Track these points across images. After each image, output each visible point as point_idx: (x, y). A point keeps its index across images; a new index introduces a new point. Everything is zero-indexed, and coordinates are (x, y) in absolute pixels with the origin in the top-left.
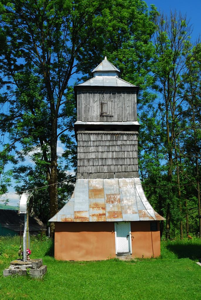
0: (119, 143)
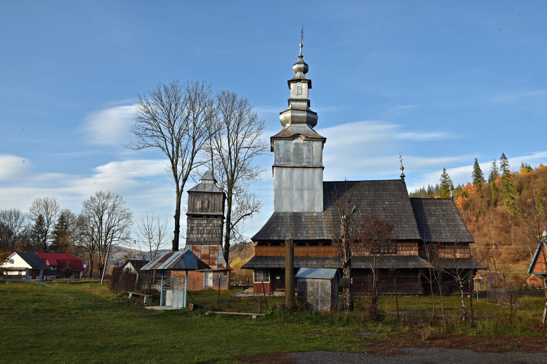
0: (211, 225)
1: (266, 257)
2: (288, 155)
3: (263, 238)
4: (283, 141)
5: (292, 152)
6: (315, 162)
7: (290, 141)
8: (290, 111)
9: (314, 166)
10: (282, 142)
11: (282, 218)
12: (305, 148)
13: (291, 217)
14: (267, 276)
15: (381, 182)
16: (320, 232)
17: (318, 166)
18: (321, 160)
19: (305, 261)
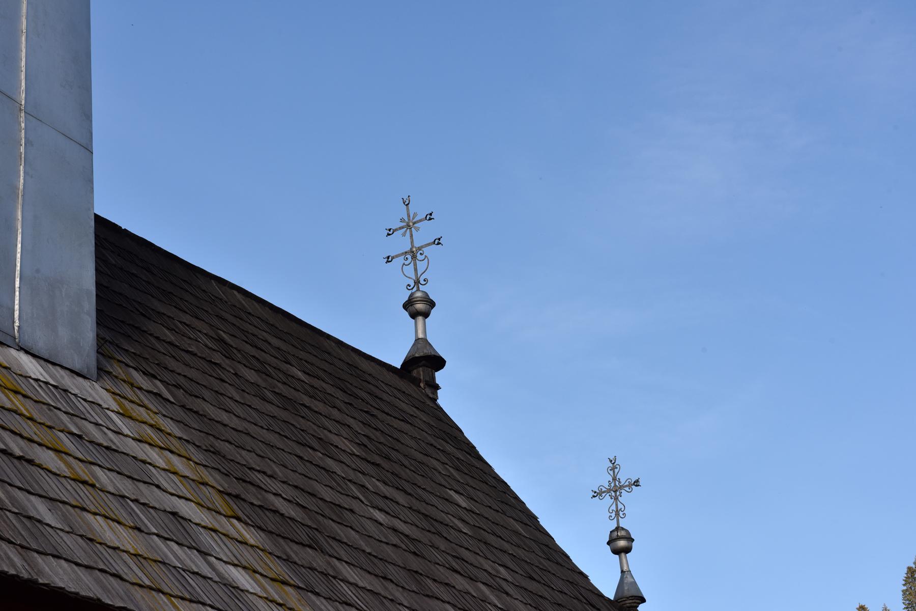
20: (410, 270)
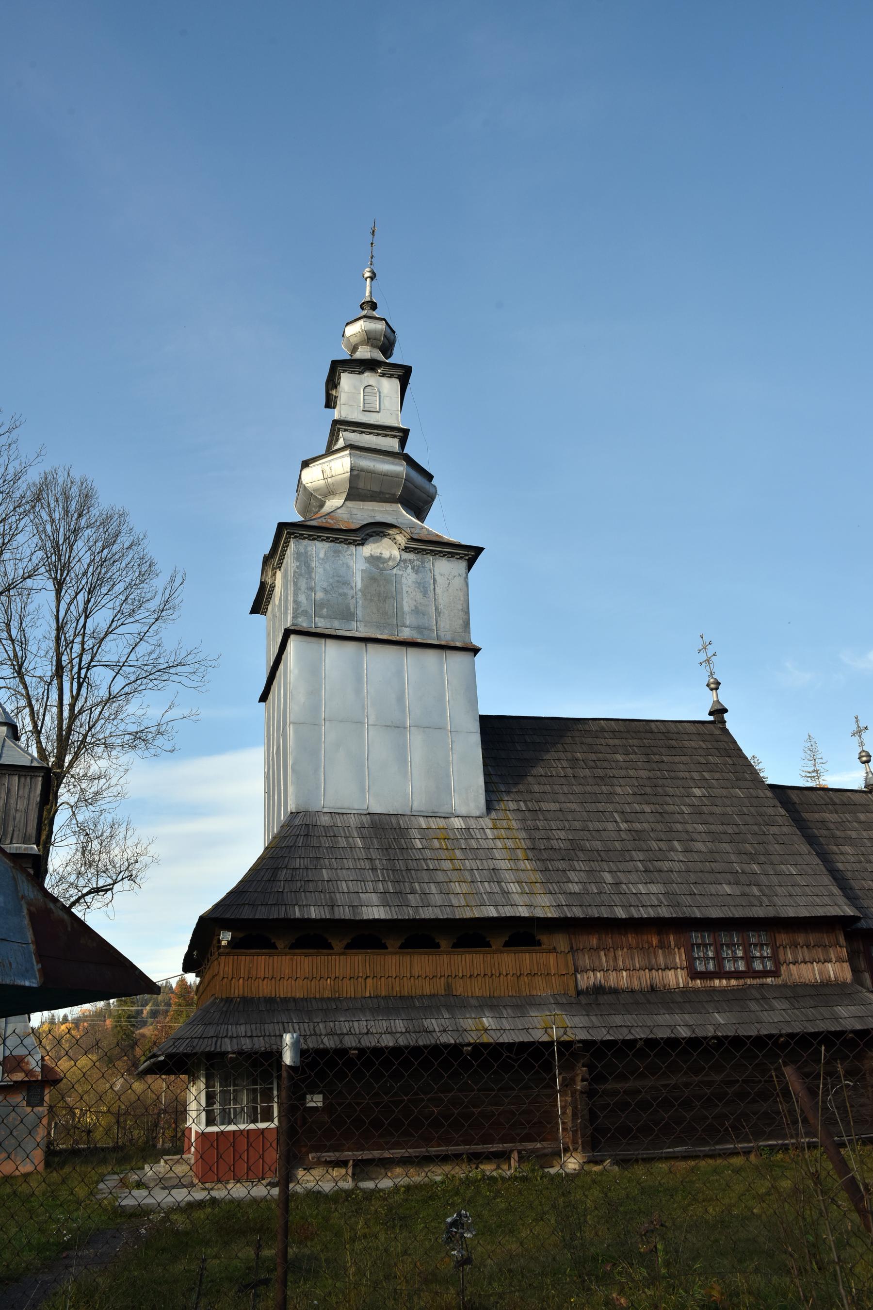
1: (270, 1001)
2: (345, 594)
3: (261, 913)
4: (327, 545)
5: (359, 585)
6: (446, 632)
7: (353, 548)
8: (347, 452)
9: (443, 643)
10: (319, 549)
11: (330, 832)
12: (408, 579)
13: (365, 832)
14: (267, 1096)
15: (653, 725)
16: (496, 888)
17: (459, 644)
18: (467, 625)
19: (446, 1016)
20: (708, 668)
